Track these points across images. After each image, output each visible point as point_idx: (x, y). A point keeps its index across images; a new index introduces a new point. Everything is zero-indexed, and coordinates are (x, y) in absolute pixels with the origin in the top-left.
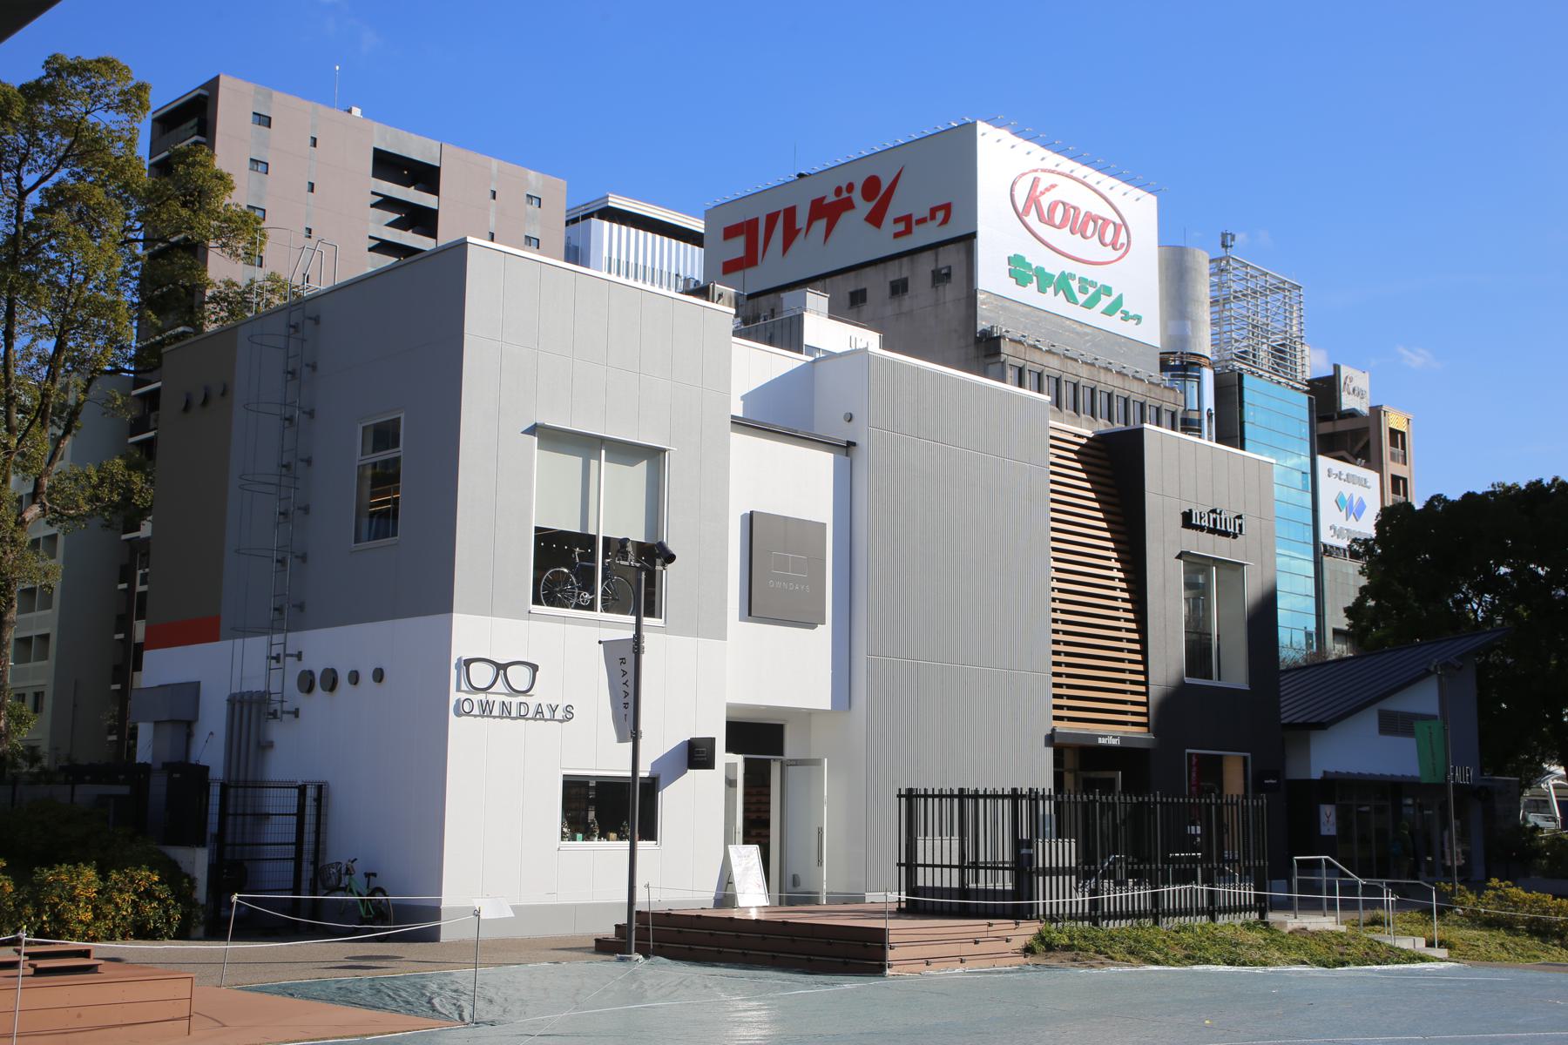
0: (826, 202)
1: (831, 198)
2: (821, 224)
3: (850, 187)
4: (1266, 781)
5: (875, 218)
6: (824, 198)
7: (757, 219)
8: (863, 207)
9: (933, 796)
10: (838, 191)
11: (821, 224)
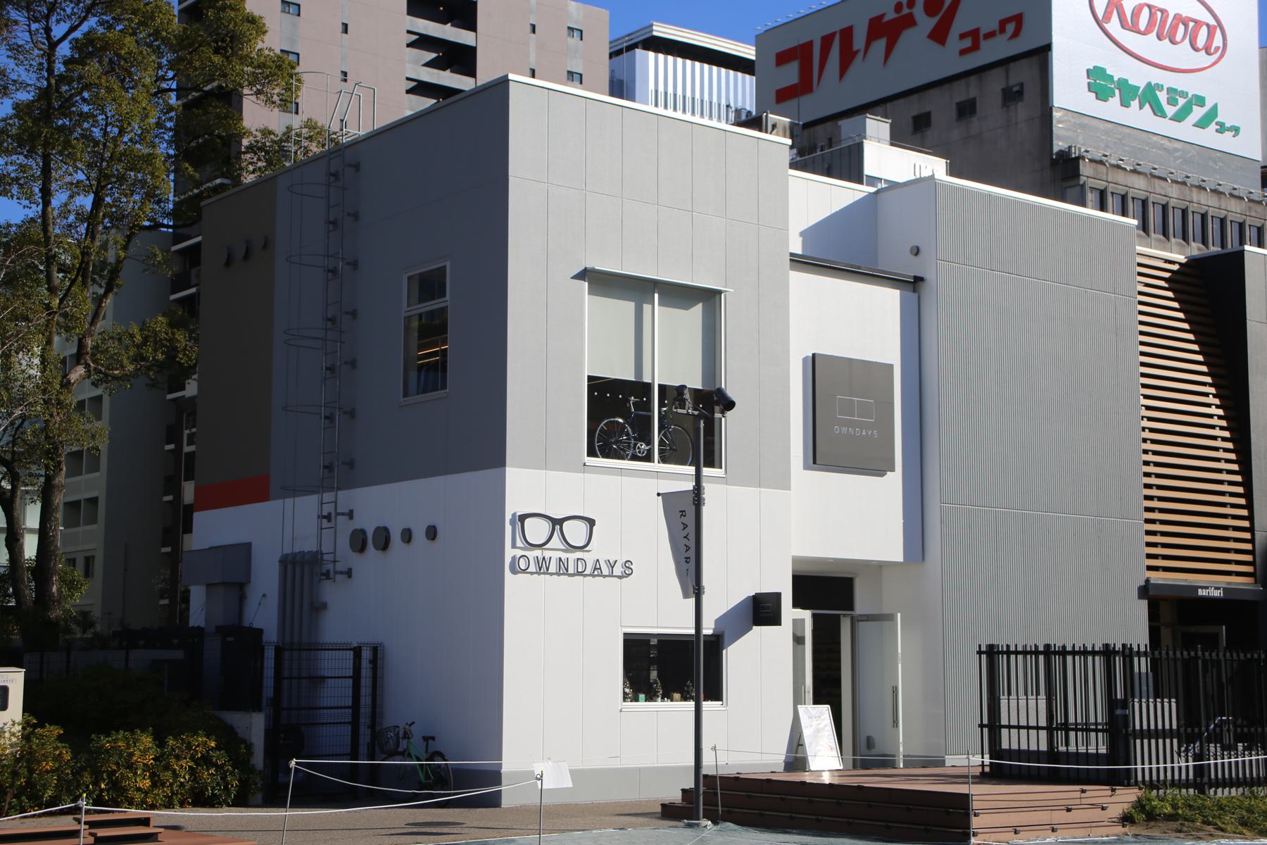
0: (886, 19)
1: (891, 15)
6: (882, 16)
11: (880, 45)
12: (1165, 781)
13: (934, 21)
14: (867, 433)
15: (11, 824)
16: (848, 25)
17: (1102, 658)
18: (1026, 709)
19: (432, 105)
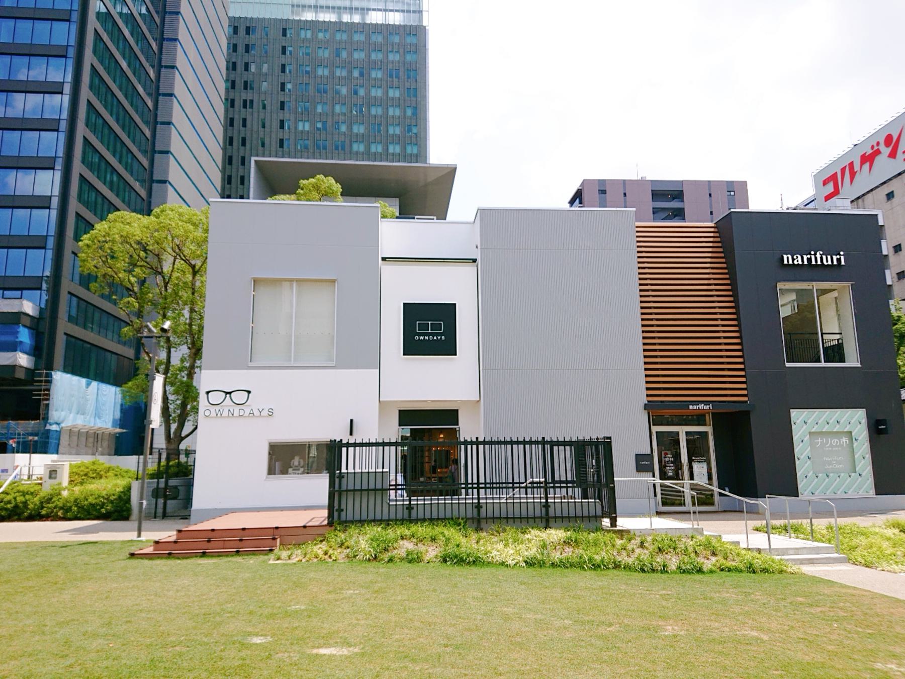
0: (867, 154)
1: (870, 151)
2: (867, 165)
3: (878, 144)
4: (880, 427)
5: (893, 155)
6: (865, 153)
7: (836, 173)
8: (886, 151)
9: (518, 443)
10: (873, 147)
11: (867, 165)
12: (478, 483)
13: (889, 150)
14: (437, 338)
15: (1, 388)
16: (851, 161)
17: (580, 489)
18: (205, 115)
19: (777, 519)
